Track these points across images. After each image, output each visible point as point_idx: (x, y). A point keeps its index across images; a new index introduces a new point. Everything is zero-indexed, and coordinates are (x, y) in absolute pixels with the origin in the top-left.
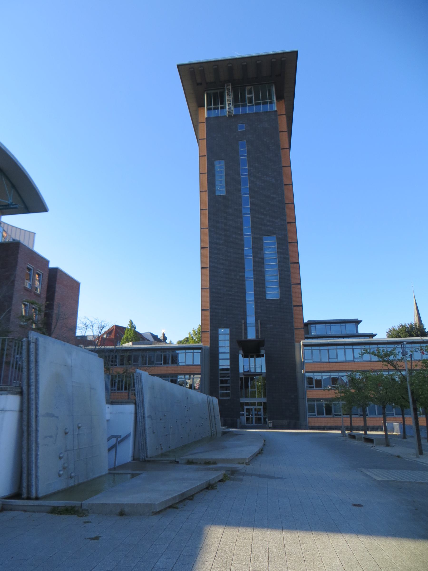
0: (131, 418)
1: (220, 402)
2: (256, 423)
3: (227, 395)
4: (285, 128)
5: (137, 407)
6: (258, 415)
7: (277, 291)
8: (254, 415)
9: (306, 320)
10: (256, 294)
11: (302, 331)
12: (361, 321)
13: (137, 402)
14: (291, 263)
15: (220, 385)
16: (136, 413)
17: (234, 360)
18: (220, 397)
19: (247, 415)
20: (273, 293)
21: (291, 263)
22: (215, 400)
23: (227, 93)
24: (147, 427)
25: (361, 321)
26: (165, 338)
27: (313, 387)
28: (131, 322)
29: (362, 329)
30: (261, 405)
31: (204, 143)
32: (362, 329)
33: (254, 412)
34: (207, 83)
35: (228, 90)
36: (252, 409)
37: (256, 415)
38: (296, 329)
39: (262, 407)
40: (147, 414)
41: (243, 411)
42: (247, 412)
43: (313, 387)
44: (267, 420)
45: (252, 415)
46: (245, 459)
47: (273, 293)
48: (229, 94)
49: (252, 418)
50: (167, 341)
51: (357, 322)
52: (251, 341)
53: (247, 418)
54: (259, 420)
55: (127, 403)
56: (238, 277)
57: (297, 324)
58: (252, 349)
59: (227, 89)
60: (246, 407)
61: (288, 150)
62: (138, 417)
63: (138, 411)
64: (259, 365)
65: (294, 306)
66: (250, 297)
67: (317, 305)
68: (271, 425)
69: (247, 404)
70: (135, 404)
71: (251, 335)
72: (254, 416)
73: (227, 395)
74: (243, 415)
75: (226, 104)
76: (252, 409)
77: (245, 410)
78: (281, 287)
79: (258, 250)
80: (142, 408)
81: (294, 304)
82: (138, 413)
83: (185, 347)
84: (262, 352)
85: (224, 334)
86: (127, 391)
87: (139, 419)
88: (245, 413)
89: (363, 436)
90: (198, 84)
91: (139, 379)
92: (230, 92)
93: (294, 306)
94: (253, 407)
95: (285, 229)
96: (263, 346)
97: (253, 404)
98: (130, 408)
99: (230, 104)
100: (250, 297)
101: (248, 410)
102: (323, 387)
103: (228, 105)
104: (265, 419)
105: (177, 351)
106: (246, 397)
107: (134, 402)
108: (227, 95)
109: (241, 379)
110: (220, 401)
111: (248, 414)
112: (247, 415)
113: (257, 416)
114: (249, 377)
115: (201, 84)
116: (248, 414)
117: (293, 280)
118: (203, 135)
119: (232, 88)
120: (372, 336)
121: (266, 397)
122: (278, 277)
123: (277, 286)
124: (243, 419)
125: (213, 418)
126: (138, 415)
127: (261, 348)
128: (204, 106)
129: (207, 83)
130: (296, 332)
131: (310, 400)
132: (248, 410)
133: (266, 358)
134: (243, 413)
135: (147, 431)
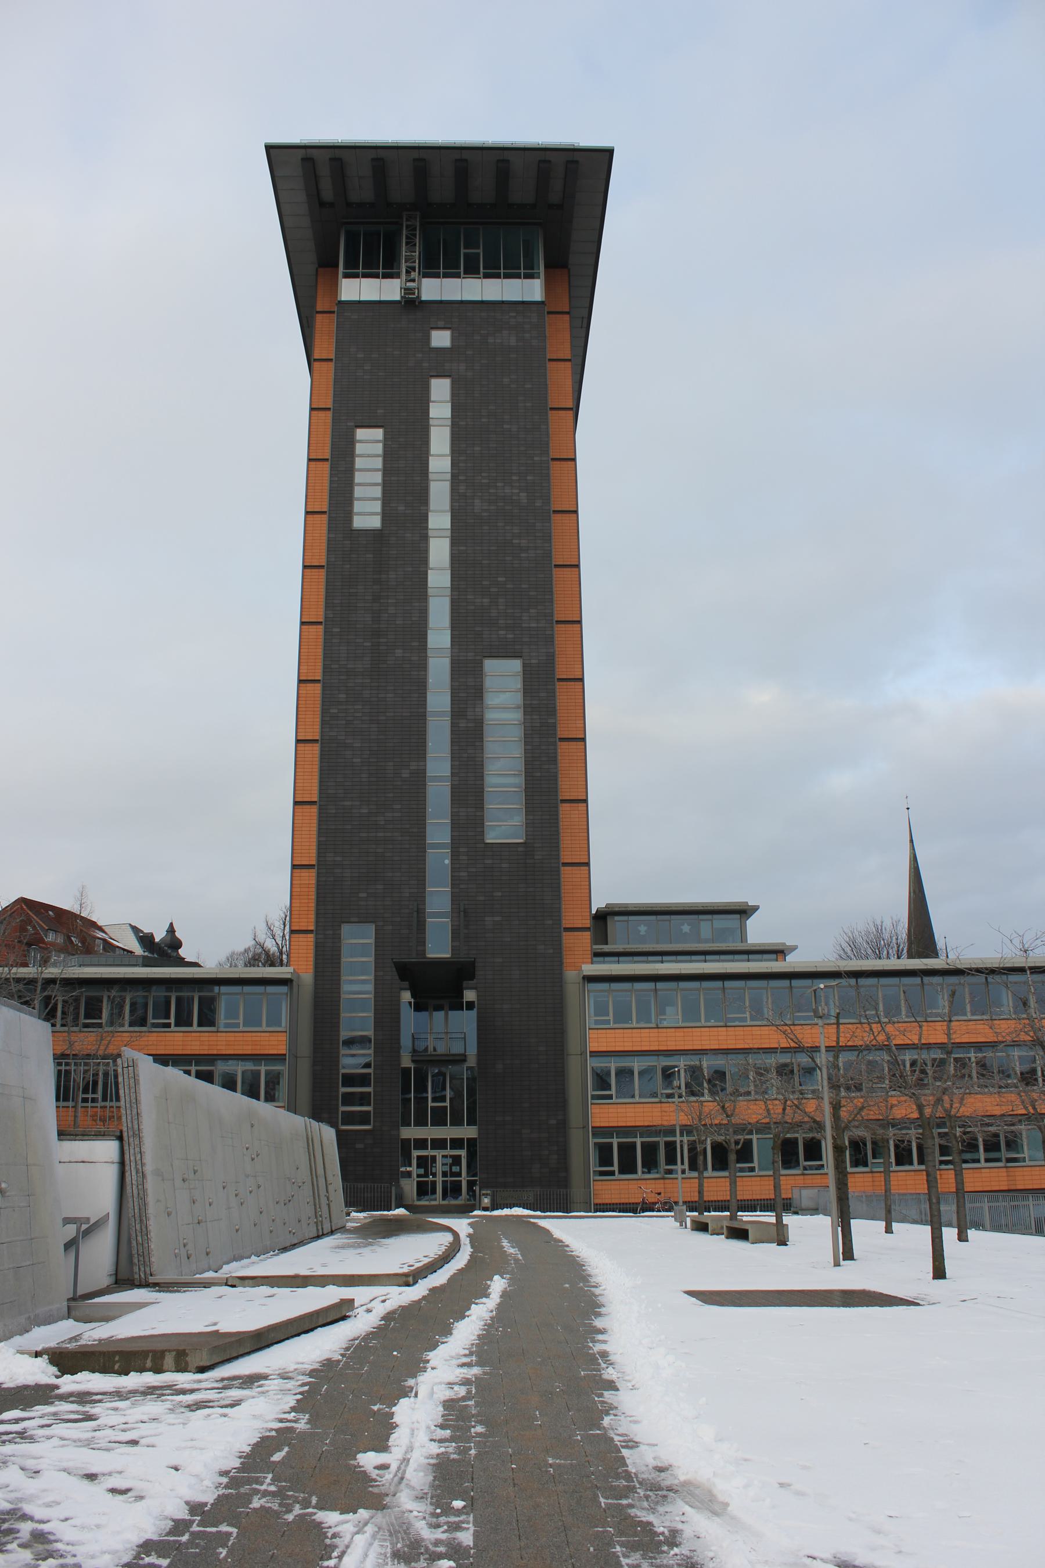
0: (109, 1176)
1: (342, 1139)
2: (444, 1197)
3: (364, 1118)
4: (565, 351)
5: (126, 1147)
6: (453, 1174)
7: (518, 820)
8: (439, 1174)
9: (598, 903)
10: (455, 825)
11: (587, 936)
12: (755, 909)
13: (125, 1135)
14: (562, 739)
15: (343, 1090)
16: (122, 1163)
17: (387, 1017)
18: (342, 1124)
19: (418, 1176)
20: (505, 824)
21: (562, 739)
22: (328, 1134)
23: (407, 237)
24: (151, 1199)
25: (755, 909)
26: (177, 944)
27: (612, 1173)
28: (171, 930)
29: (758, 931)
30: (461, 1147)
31: (328, 370)
32: (758, 931)
33: (439, 1168)
34: (352, 209)
35: (411, 229)
36: (434, 1158)
37: (444, 1174)
38: (567, 929)
39: (463, 1153)
40: (149, 1169)
41: (410, 1166)
42: (419, 1166)
43: (612, 1173)
44: (477, 1188)
45: (434, 1175)
46: (206, 1504)
47: (505, 824)
48: (410, 243)
49: (434, 1183)
50: (182, 952)
51: (744, 912)
52: (439, 964)
53: (420, 1184)
54: (453, 1190)
55: (99, 1135)
56: (405, 774)
57: (573, 916)
58: (436, 986)
59: (407, 227)
60: (415, 1153)
61: (571, 413)
62: (127, 1174)
63: (127, 1157)
64: (456, 1031)
65: (565, 864)
66: (439, 831)
67: (634, 849)
68: (486, 1201)
69: (421, 1144)
70: (120, 1138)
71: (439, 947)
72: (439, 1179)
73: (364, 1118)
74: (409, 1174)
75: (399, 268)
76: (434, 1158)
77: (414, 1162)
78: (530, 808)
79: (468, 691)
80: (138, 1150)
81: (566, 857)
82: (127, 1162)
83: (256, 979)
84: (470, 995)
85: (359, 944)
86: (71, 1104)
87: (131, 1177)
88: (413, 1169)
89: (726, 1224)
90: (322, 204)
91: (132, 1075)
92: (415, 235)
93: (565, 864)
94: (438, 1154)
95: (550, 640)
96: (472, 977)
97: (439, 1144)
98: (108, 1149)
99: (414, 269)
100: (439, 831)
101: (422, 1162)
102: (796, 1135)
103: (408, 272)
104: (471, 1184)
105: (216, 989)
106: (421, 1122)
107: (118, 1134)
108: (407, 244)
109: (406, 1071)
110: (341, 1136)
111: (422, 1171)
112: (418, 1176)
113: (449, 1179)
114: (431, 1065)
115: (332, 205)
116: (422, 1171)
117: (566, 790)
118: (325, 348)
119: (421, 225)
120: (779, 952)
121: (402, 1140)
122: (521, 781)
123: (518, 804)
124: (410, 1187)
125: (322, 1181)
126: (127, 1168)
127: (465, 984)
128: (337, 266)
129: (352, 209)
130: (567, 938)
131: (598, 1131)
132: (422, 1162)
133: (478, 1013)
134: (408, 1169)
135: (151, 1210)
